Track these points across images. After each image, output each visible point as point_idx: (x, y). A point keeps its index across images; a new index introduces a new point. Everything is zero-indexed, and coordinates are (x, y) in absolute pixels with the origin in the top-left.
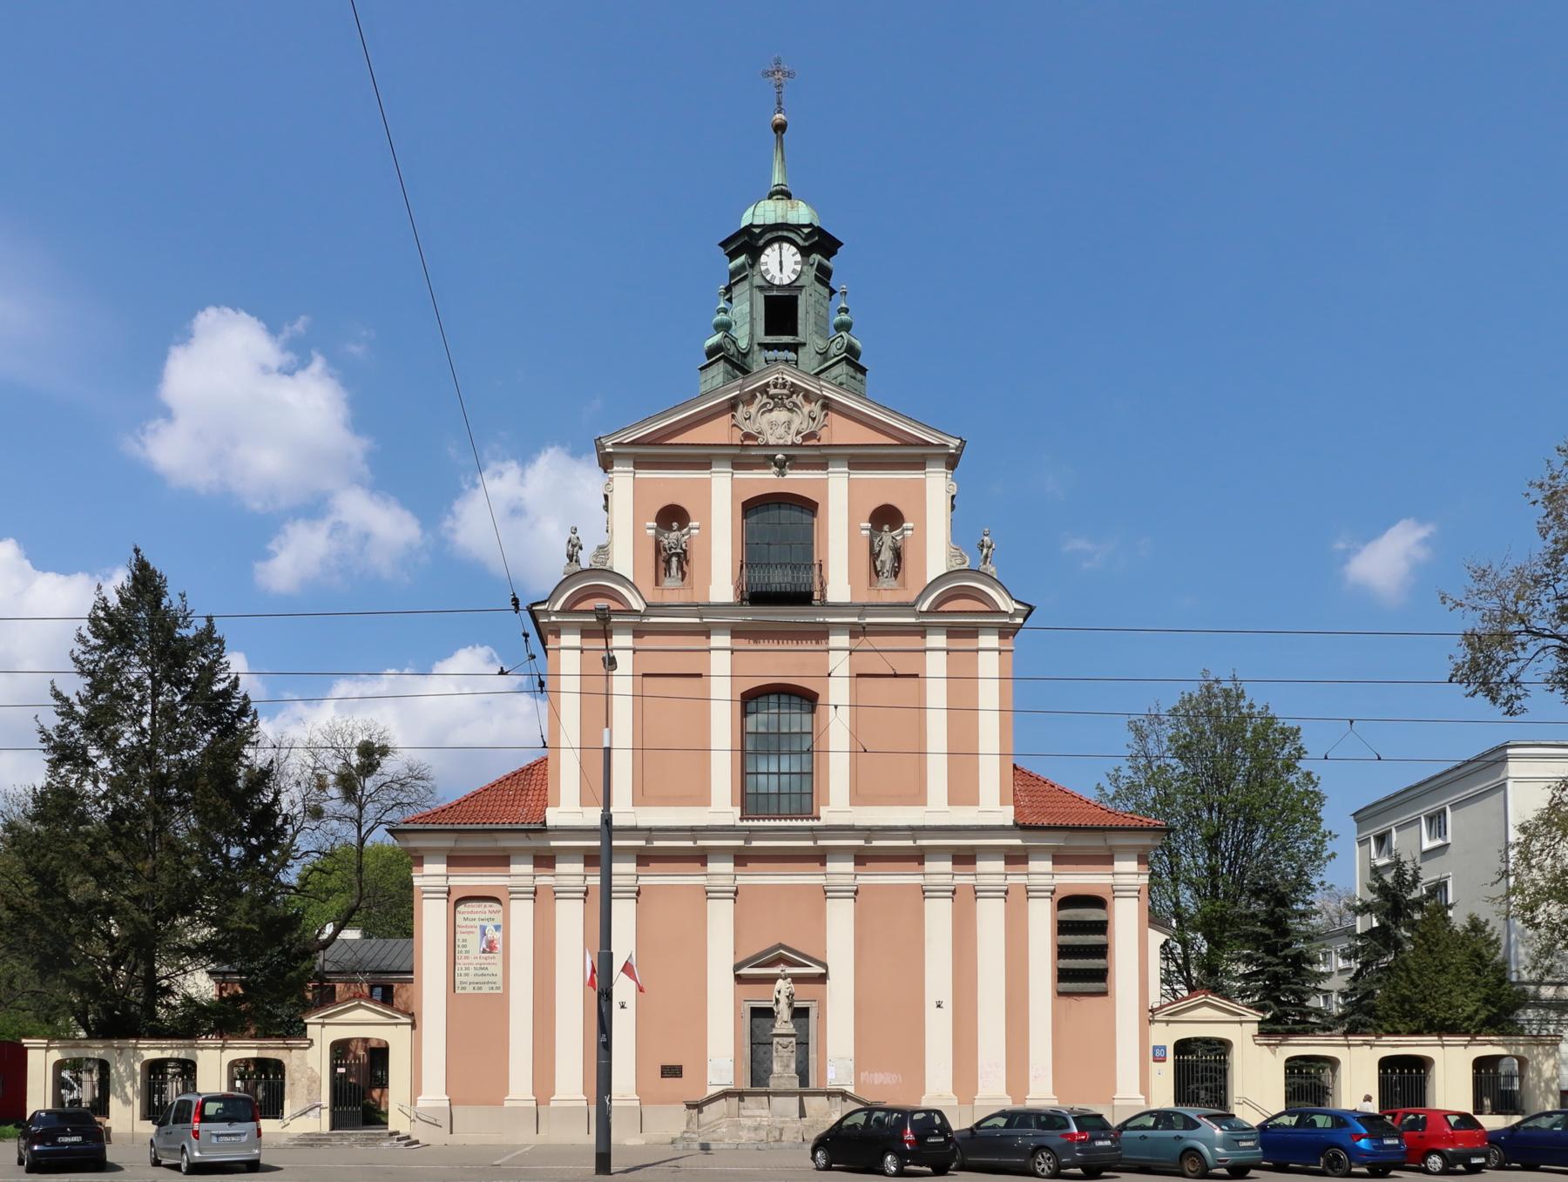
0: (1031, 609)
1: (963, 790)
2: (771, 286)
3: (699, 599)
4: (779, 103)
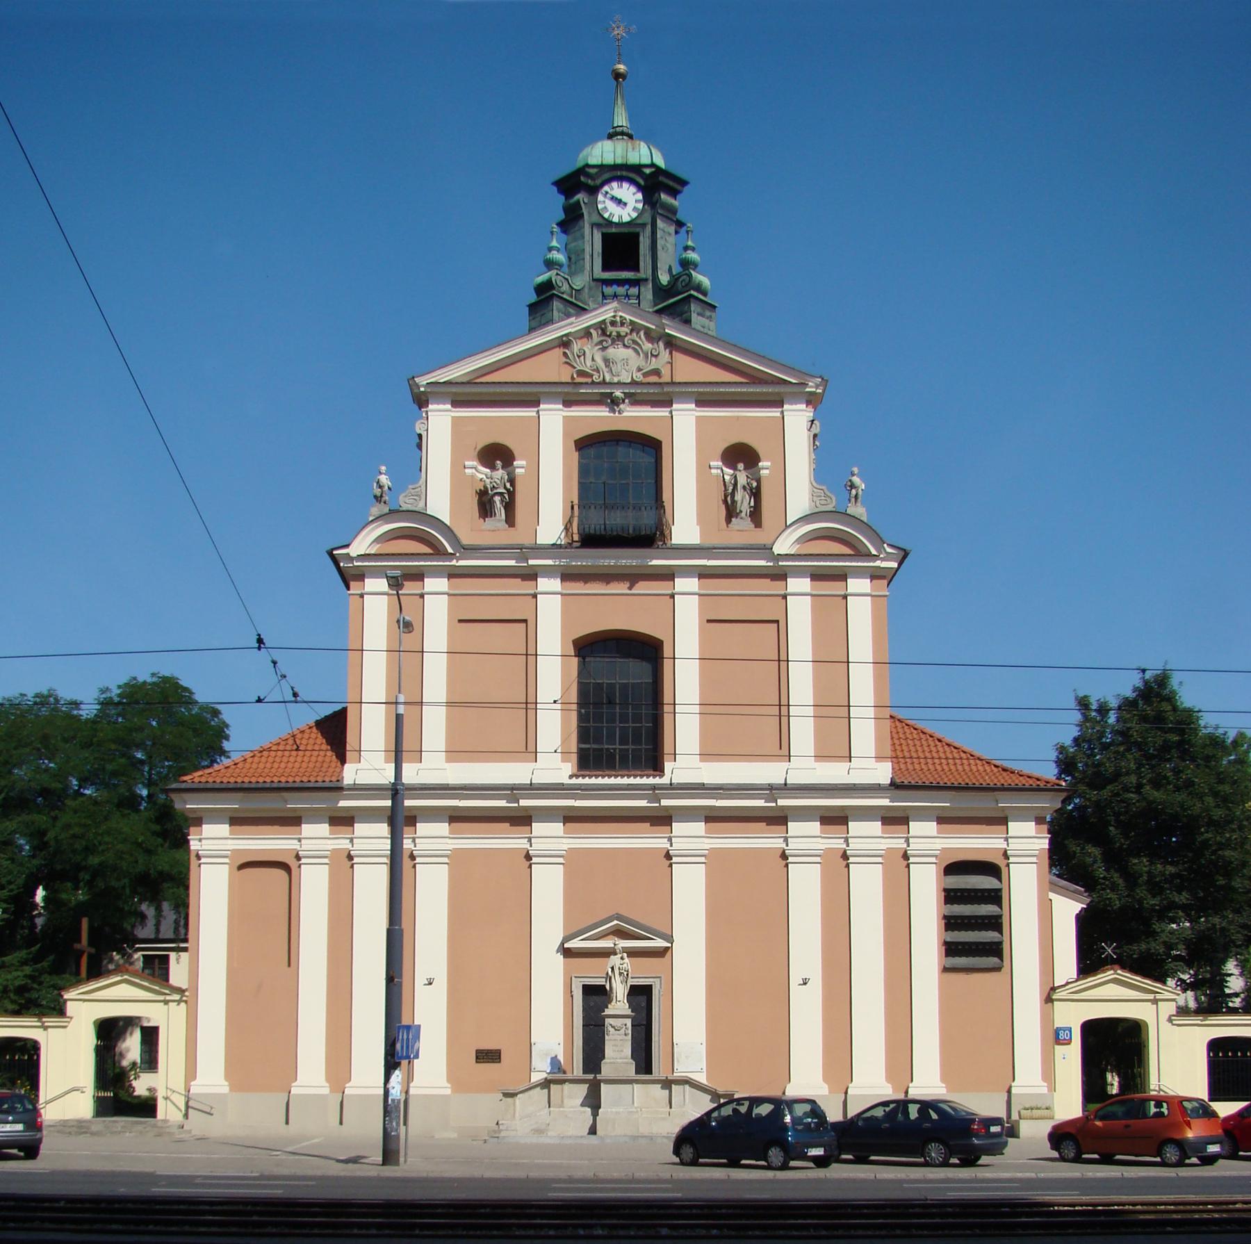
1: (835, 746)
2: (609, 223)
3: (527, 541)
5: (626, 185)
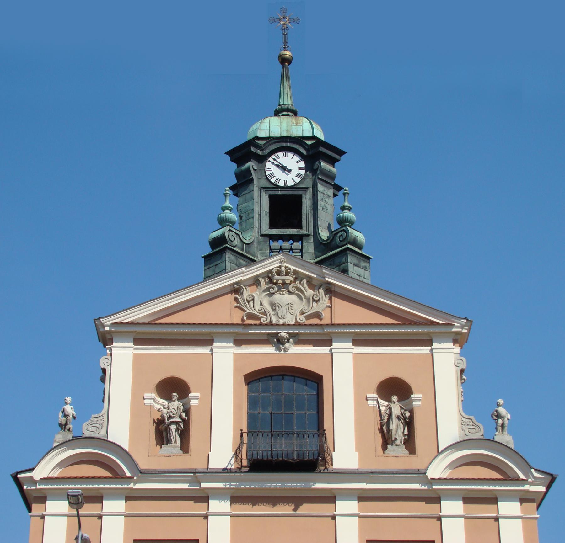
0: (553, 479)
2: (276, 187)
3: (200, 466)
4: (285, 42)
5: (290, 155)
